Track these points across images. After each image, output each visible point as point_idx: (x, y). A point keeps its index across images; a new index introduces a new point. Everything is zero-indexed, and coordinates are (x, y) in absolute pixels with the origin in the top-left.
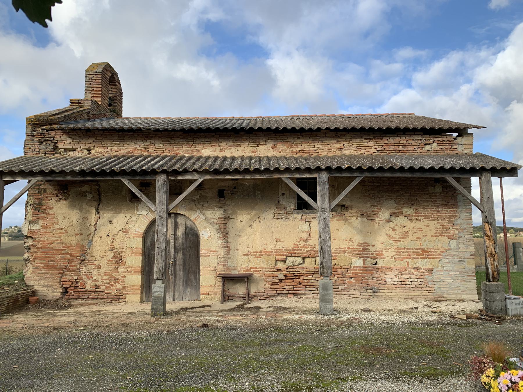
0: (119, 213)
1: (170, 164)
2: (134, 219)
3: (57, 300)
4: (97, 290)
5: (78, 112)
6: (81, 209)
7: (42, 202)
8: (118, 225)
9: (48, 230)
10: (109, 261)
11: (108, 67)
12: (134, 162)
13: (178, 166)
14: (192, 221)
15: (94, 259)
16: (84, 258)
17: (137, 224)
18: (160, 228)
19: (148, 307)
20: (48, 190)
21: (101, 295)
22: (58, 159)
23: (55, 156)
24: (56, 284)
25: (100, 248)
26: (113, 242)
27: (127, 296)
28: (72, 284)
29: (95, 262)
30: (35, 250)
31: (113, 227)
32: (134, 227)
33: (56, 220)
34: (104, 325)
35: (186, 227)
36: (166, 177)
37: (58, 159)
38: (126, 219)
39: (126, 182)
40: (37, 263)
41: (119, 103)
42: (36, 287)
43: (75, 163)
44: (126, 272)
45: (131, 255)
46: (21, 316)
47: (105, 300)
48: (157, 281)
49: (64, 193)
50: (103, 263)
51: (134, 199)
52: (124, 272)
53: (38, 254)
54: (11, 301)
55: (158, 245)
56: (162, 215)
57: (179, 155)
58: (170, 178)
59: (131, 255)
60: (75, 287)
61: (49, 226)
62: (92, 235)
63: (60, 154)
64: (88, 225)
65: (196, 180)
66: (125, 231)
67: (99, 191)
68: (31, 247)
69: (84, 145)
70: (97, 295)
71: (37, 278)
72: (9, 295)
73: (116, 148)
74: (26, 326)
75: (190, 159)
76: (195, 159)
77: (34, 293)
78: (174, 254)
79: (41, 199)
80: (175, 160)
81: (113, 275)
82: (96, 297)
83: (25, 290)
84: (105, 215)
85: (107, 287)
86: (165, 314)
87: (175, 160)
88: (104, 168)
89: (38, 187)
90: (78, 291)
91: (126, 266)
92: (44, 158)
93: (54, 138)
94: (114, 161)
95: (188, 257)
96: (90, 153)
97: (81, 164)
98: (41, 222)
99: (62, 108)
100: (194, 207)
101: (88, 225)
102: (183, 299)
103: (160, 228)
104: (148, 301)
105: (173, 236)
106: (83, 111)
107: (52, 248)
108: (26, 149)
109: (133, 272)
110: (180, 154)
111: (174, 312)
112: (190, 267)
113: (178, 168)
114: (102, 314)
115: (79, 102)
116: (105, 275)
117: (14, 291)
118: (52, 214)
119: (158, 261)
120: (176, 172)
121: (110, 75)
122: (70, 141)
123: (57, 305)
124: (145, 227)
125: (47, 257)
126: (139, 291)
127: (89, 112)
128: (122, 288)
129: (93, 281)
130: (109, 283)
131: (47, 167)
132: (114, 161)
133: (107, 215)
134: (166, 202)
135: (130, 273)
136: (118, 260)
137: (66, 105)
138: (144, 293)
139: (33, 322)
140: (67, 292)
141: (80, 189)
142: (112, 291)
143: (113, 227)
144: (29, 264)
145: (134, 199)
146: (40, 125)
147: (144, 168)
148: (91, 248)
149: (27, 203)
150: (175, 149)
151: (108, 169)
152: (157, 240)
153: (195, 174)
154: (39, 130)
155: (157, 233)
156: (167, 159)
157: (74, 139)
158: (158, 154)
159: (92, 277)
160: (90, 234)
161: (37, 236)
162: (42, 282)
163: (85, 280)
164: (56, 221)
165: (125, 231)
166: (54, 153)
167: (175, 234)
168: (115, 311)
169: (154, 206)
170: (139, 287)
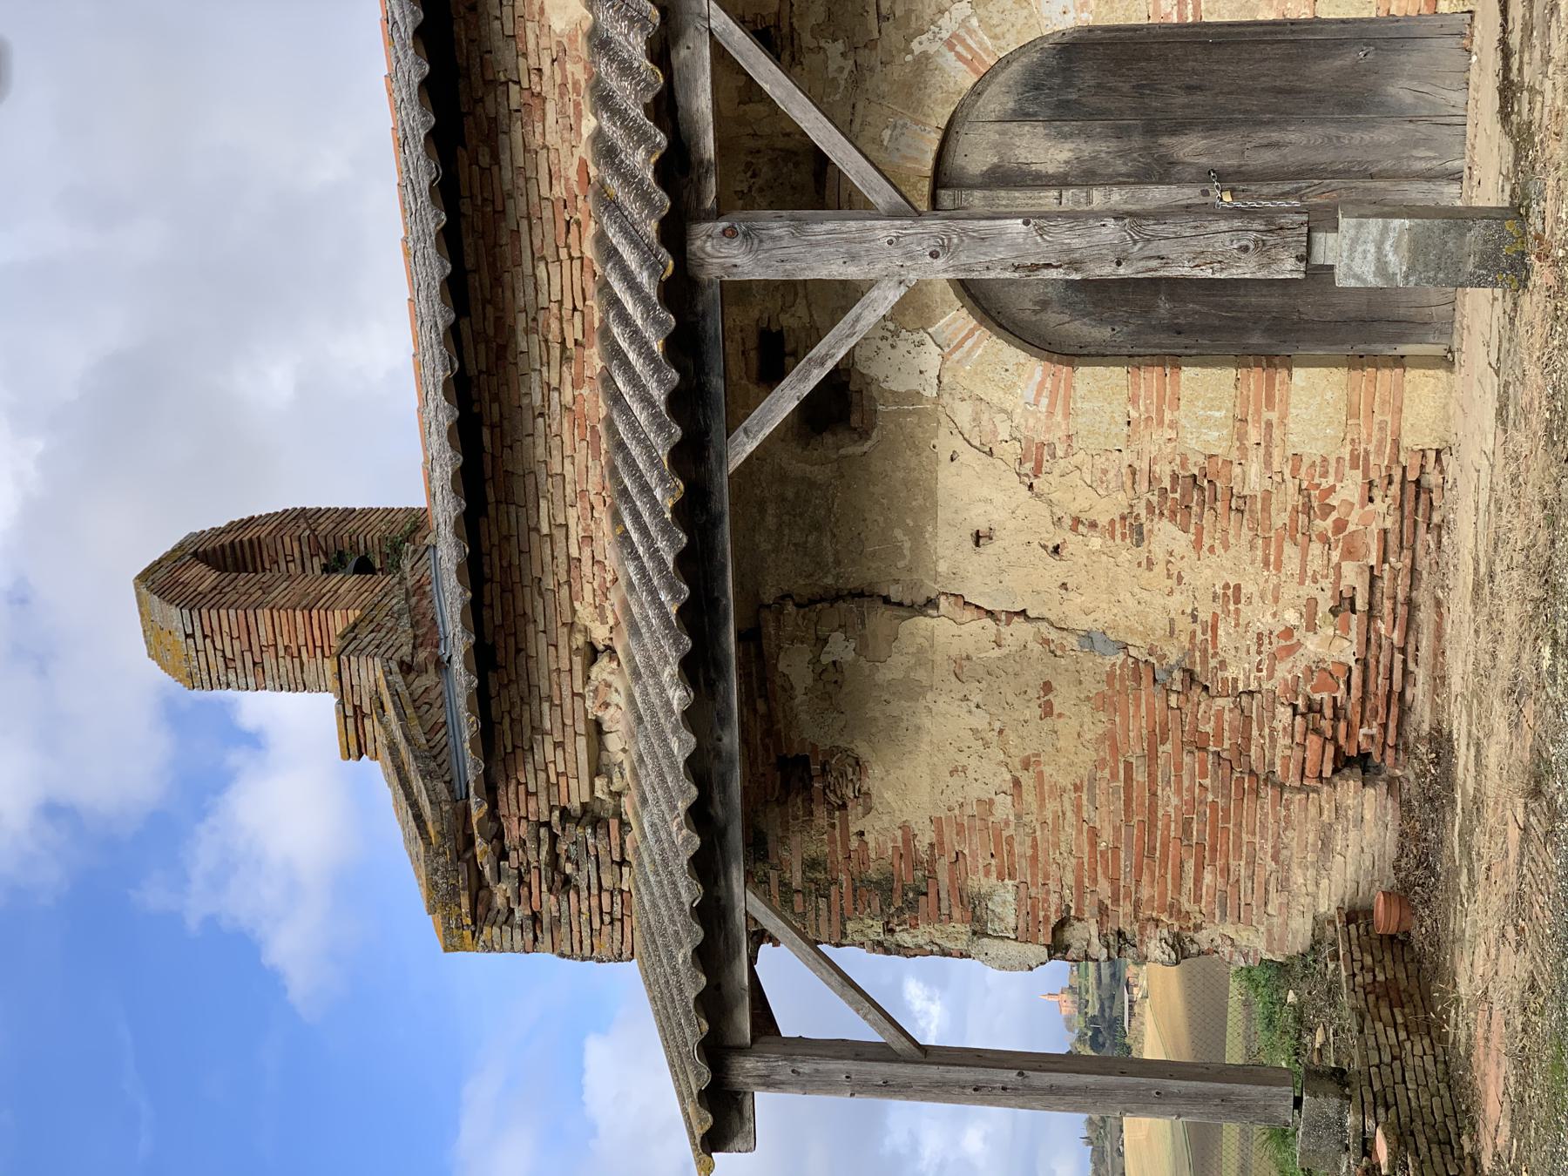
0: (931, 493)
1: (633, 208)
2: (964, 414)
3: (1406, 806)
4: (1361, 604)
5: (402, 716)
6: (913, 691)
7: (875, 877)
8: (998, 498)
9: (1022, 848)
10: (1198, 544)
11: (162, 580)
12: (636, 408)
13: (641, 154)
14: (985, 79)
15: (1183, 624)
16: (1177, 675)
17: (995, 396)
18: (1001, 253)
19: (1480, 309)
20: (813, 850)
21: (1393, 585)
22: (644, 801)
23: (630, 816)
24: (1313, 811)
25: (1137, 595)
26: (1093, 525)
27: (1406, 441)
28: (1317, 731)
29: (1205, 615)
30: (1126, 908)
31: (1010, 525)
32: (1010, 415)
33: (968, 811)
34: (1543, 537)
35: (1021, 115)
36: (707, 226)
37: (644, 801)
38: (968, 455)
39: (743, 448)
40: (1198, 899)
41: (353, 525)
42: (1327, 906)
43: (654, 715)
44: (1268, 455)
45: (1173, 425)
46: (1462, 968)
47: (1423, 563)
48: (1319, 258)
49: (824, 772)
50: (1209, 573)
51: (840, 405)
52: (1268, 464)
53: (1145, 893)
54: (1385, 1012)
55: (1101, 259)
56: (930, 244)
57: (593, 171)
58: (710, 202)
59: (1173, 425)
60: (1336, 718)
61: (1000, 844)
62: (1054, 635)
63: (619, 794)
64: (997, 653)
65: (720, 53)
66: (1035, 462)
67: (812, 602)
68: (1111, 926)
69: (565, 678)
70: (1391, 612)
71: (1275, 899)
72: (1352, 1023)
73: (572, 513)
74: (1511, 932)
75: (604, 100)
76: (603, 66)
77: (1355, 915)
78: (1180, 182)
79: (861, 886)
80: (614, 185)
81: (1280, 519)
82: (1402, 611)
83: (1335, 956)
84: (943, 567)
85: (1349, 554)
86: (1517, 211)
87: (614, 185)
88: (670, 560)
89: (798, 898)
90: (1363, 700)
91: (1234, 455)
92: (640, 864)
93: (540, 824)
94: (636, 516)
95: (1198, 98)
96: (610, 649)
97: (659, 684)
98: (979, 882)
99: (389, 792)
100: (896, 72)
101: (997, 653)
102: (1457, 124)
103: (1007, 242)
104: (1446, 326)
105: (1068, 194)
106: (395, 694)
107: (1117, 830)
108: (606, 952)
109: (1267, 415)
110: (583, 164)
111: (1517, 160)
112: (1265, 82)
113: (650, 153)
114: (1491, 563)
115: (353, 718)
116: (1279, 565)
117: (1333, 1005)
118: (940, 832)
119: (1198, 257)
120: (676, 167)
121: (200, 568)
122: (549, 748)
123: (1427, 805)
124: (1012, 355)
125: (1165, 854)
126: (1385, 376)
127: (401, 663)
128: (1358, 475)
129: (1312, 627)
130: (1324, 539)
131: (679, 841)
132: (636, 516)
133: (948, 558)
134: (853, 225)
135: (1276, 433)
136: (1196, 493)
137: (374, 772)
138: (1403, 349)
139: (1496, 902)
140: (1364, 757)
141: (800, 698)
142: (1375, 528)
143: (1010, 525)
144: (1203, 937)
145: (855, 419)
146: (479, 889)
147: (657, 346)
148: (1122, 637)
149: (880, 947)
150: (559, 191)
151: (672, 541)
152: (1074, 265)
153: (681, 55)
154: (502, 892)
155: (1035, 267)
156: (613, 233)
157: (537, 729)
158: (591, 288)
159: (1288, 632)
160: (1046, 642)
161: (1054, 898)
162: (1298, 877)
163: (1302, 664)
164: (972, 809)
165: (1035, 462)
166: (614, 824)
167: (1061, 182)
168: (1484, 496)
169: (874, 293)
170: (1362, 377)
